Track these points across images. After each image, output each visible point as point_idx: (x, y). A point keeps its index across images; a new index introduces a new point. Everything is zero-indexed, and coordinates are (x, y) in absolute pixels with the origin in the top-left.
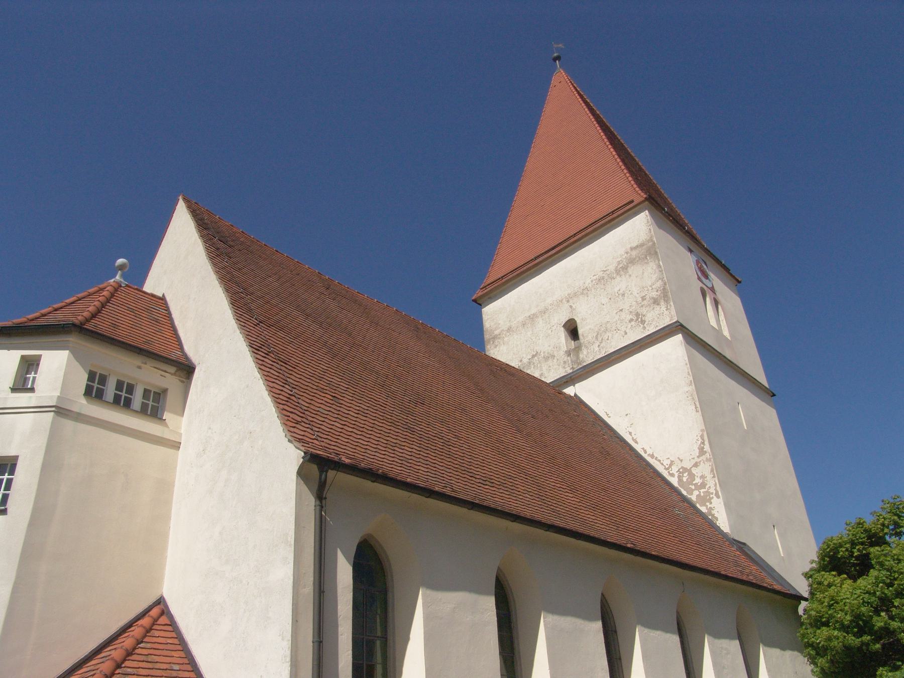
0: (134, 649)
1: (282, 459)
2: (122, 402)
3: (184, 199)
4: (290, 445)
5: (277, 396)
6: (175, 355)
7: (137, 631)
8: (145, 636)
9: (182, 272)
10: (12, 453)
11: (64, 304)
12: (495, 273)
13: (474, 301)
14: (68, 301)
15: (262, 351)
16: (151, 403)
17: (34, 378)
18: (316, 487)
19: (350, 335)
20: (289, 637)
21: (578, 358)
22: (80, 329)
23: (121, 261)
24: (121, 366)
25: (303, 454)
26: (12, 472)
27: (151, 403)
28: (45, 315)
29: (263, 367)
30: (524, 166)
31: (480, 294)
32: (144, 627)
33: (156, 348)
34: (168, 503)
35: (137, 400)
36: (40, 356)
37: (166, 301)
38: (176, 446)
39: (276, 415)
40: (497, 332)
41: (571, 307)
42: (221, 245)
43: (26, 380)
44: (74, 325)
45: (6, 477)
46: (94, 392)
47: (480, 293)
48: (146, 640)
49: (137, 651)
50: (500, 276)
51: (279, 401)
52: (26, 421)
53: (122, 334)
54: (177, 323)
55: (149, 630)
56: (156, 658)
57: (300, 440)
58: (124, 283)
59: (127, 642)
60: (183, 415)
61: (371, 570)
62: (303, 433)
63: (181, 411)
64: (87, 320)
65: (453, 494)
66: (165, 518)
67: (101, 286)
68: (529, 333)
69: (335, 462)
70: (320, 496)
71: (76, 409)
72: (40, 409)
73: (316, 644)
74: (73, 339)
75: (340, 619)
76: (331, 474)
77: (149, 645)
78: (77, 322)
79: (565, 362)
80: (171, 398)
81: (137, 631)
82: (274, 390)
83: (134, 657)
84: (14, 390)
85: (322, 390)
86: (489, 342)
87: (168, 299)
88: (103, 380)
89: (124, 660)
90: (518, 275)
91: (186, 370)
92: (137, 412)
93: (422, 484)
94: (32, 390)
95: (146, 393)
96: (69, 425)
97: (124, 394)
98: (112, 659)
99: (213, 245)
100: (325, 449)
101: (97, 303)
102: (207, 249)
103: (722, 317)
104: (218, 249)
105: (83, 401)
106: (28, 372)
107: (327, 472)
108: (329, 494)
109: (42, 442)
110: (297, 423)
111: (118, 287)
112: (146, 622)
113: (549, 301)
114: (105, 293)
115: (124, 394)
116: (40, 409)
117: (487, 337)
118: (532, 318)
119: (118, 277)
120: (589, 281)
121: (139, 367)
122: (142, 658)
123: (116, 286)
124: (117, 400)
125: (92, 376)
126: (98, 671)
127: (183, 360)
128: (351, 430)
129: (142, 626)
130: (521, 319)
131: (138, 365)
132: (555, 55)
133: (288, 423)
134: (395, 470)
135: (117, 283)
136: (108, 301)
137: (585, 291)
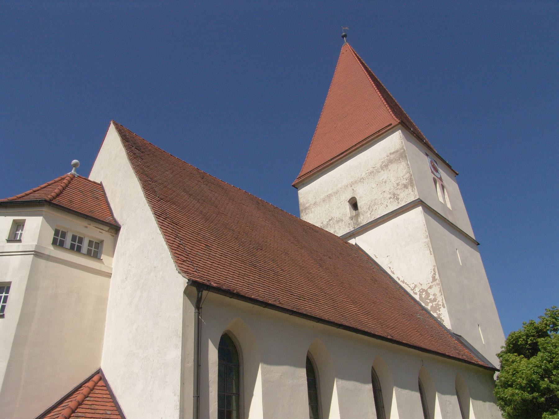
0: (83, 401)
1: (174, 284)
2: (76, 248)
3: (114, 123)
4: (180, 275)
5: (171, 245)
6: (108, 219)
7: (84, 390)
8: (90, 393)
9: (113, 168)
10: (8, 280)
11: (39, 188)
12: (306, 169)
13: (293, 186)
14: (42, 186)
15: (162, 217)
16: (93, 249)
17: (21, 234)
18: (195, 301)
19: (216, 207)
20: (179, 394)
21: (357, 221)
22: (49, 203)
23: (75, 161)
24: (75, 226)
25: (187, 280)
26: (7, 292)
27: (93, 249)
28: (28, 195)
29: (162, 227)
30: (324, 103)
31: (297, 181)
32: (89, 388)
33: (97, 215)
34: (104, 311)
35: (85, 247)
36: (25, 220)
37: (103, 186)
38: (109, 275)
39: (171, 257)
40: (307, 205)
41: (353, 189)
42: (137, 151)
43: (16, 235)
44: (46, 201)
45: (4, 294)
46: (58, 242)
47: (297, 181)
48: (90, 395)
49: (85, 402)
50: (309, 171)
51: (172, 248)
52: (16, 260)
53: (75, 207)
54: (109, 199)
55: (92, 389)
56: (96, 407)
57: (185, 272)
58: (77, 175)
59: (79, 397)
60: (113, 257)
61: (230, 352)
62: (187, 268)
63: (112, 254)
64: (54, 198)
65: (280, 305)
66: (102, 320)
67: (63, 177)
68: (327, 206)
69: (207, 285)
70: (198, 307)
71: (47, 253)
72: (25, 253)
73: (196, 398)
74: (45, 209)
75: (210, 383)
76: (205, 293)
77: (92, 399)
78: (47, 199)
79: (349, 224)
80: (106, 246)
81: (84, 390)
82: (169, 241)
83: (83, 406)
84: (9, 241)
85: (199, 241)
86: (302, 211)
87: (104, 185)
88: (64, 235)
89: (77, 408)
90: (320, 170)
91: (115, 228)
92: (85, 254)
93: (261, 299)
94: (20, 241)
95: (91, 243)
96: (42, 263)
97: (76, 244)
98: (69, 407)
99: (132, 151)
100: (201, 277)
101: (60, 187)
102: (128, 154)
103: (446, 196)
104: (135, 154)
105: (52, 248)
106: (17, 230)
107: (202, 291)
108: (203, 305)
109: (26, 273)
110: (184, 261)
111: (73, 178)
112: (90, 384)
113: (340, 186)
114: (65, 181)
115: (76, 244)
116: (25, 253)
117: (301, 208)
118: (329, 197)
119: (73, 171)
120: (364, 174)
121: (86, 227)
122: (88, 406)
123: (72, 177)
124: (72, 247)
125: (57, 232)
126: (61, 415)
127: (113, 223)
128: (217, 266)
129: (88, 387)
130: (322, 197)
131: (86, 226)
132: (343, 34)
133: (178, 261)
134: (244, 291)
135: (72, 175)
136: (67, 186)
137: (362, 180)
